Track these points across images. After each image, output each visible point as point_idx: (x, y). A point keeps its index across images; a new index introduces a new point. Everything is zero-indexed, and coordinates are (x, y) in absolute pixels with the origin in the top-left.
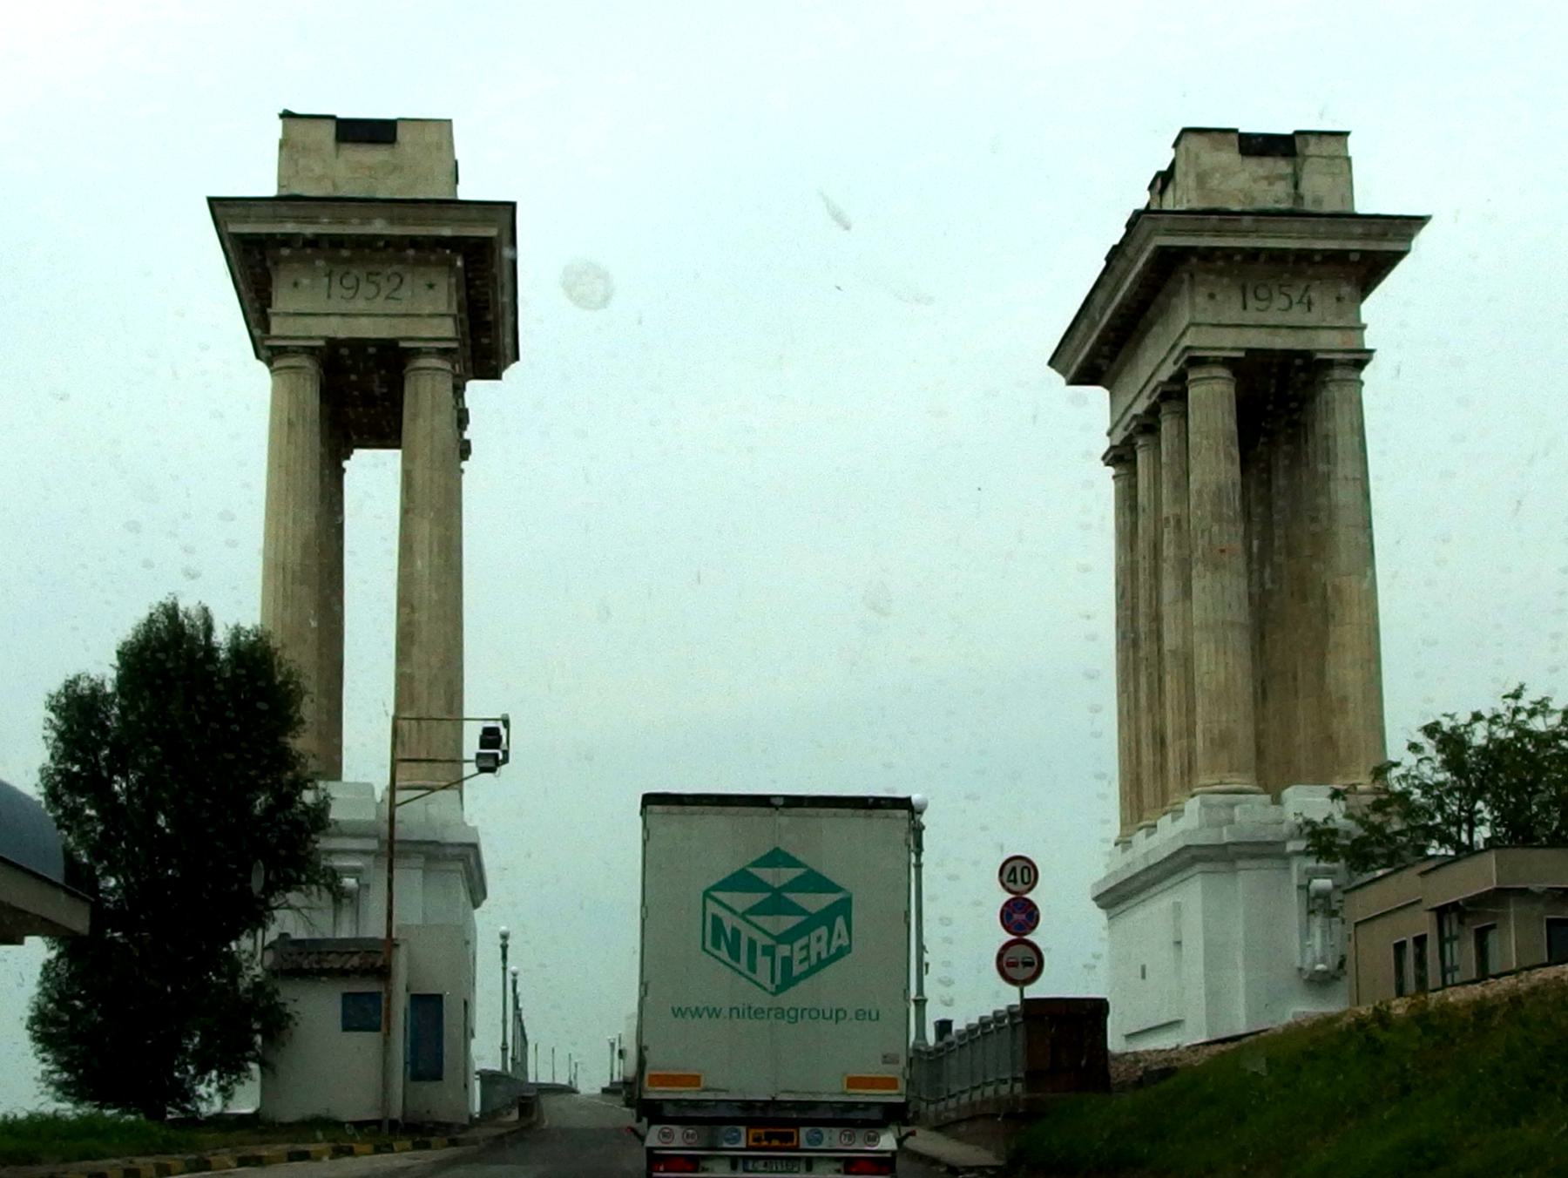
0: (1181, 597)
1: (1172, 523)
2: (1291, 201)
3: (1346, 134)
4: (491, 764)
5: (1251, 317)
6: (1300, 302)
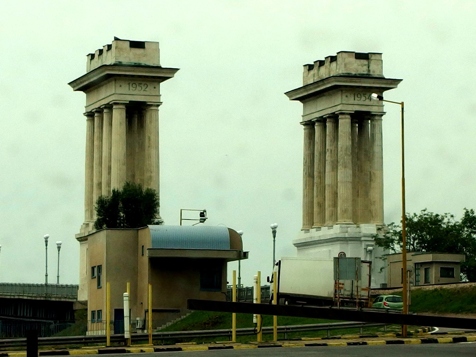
0: (331, 171)
1: (329, 151)
2: (367, 72)
3: (381, 54)
4: (202, 221)
5: (356, 102)
6: (368, 99)
